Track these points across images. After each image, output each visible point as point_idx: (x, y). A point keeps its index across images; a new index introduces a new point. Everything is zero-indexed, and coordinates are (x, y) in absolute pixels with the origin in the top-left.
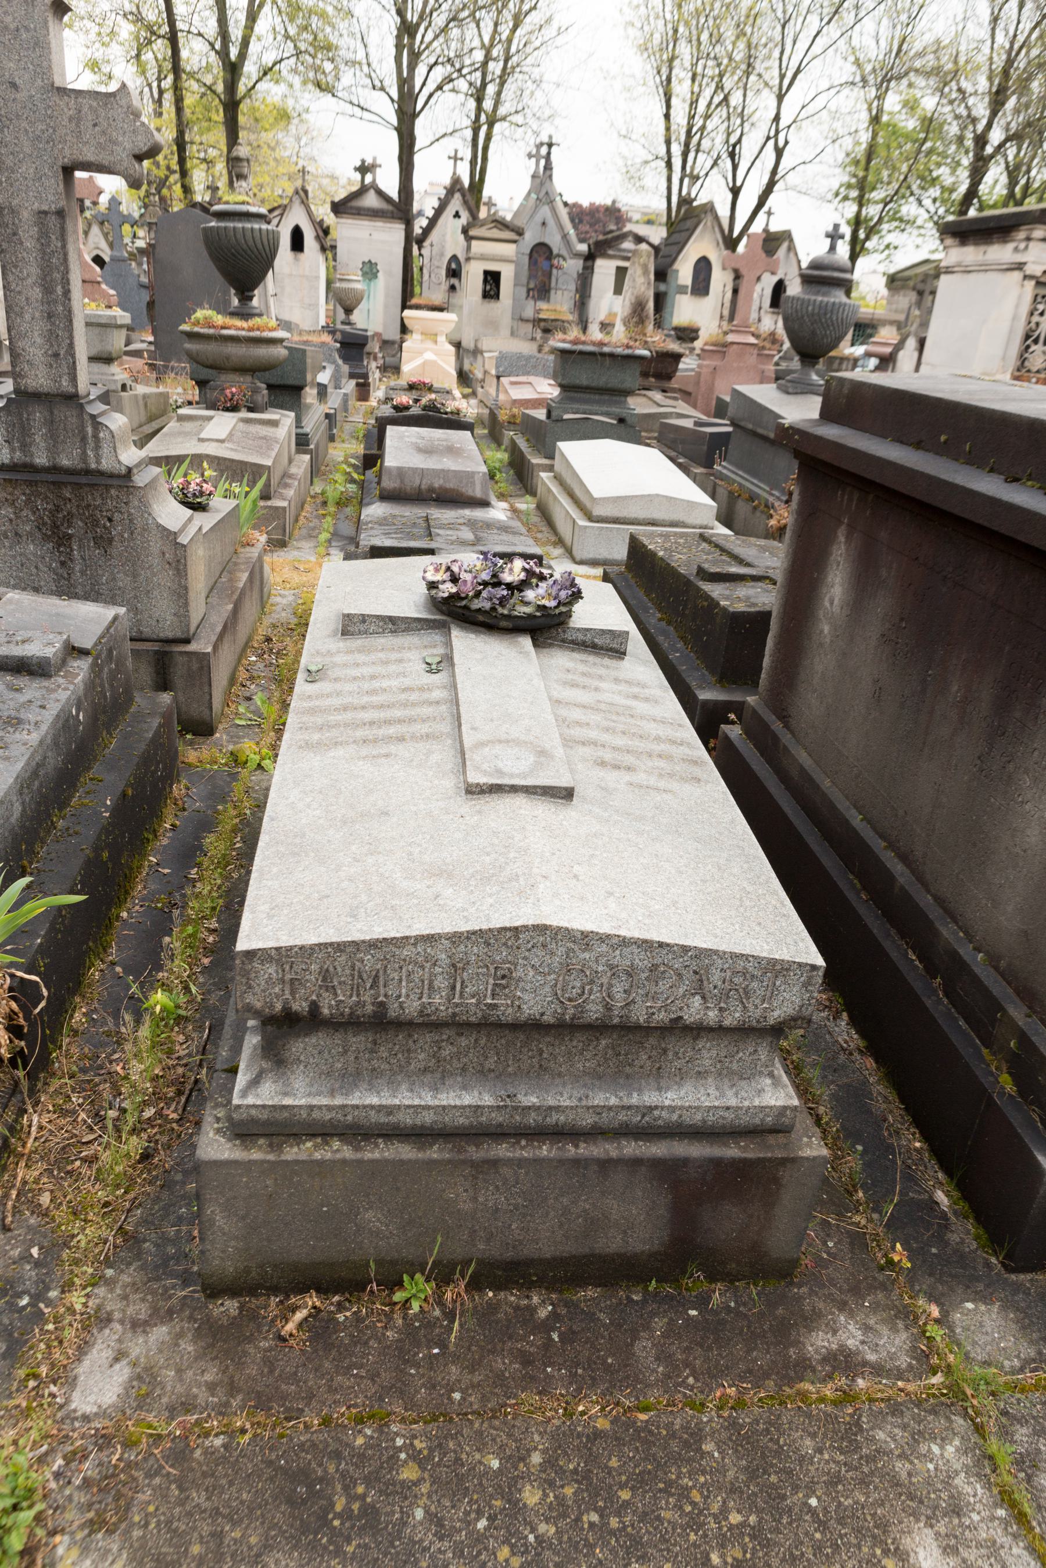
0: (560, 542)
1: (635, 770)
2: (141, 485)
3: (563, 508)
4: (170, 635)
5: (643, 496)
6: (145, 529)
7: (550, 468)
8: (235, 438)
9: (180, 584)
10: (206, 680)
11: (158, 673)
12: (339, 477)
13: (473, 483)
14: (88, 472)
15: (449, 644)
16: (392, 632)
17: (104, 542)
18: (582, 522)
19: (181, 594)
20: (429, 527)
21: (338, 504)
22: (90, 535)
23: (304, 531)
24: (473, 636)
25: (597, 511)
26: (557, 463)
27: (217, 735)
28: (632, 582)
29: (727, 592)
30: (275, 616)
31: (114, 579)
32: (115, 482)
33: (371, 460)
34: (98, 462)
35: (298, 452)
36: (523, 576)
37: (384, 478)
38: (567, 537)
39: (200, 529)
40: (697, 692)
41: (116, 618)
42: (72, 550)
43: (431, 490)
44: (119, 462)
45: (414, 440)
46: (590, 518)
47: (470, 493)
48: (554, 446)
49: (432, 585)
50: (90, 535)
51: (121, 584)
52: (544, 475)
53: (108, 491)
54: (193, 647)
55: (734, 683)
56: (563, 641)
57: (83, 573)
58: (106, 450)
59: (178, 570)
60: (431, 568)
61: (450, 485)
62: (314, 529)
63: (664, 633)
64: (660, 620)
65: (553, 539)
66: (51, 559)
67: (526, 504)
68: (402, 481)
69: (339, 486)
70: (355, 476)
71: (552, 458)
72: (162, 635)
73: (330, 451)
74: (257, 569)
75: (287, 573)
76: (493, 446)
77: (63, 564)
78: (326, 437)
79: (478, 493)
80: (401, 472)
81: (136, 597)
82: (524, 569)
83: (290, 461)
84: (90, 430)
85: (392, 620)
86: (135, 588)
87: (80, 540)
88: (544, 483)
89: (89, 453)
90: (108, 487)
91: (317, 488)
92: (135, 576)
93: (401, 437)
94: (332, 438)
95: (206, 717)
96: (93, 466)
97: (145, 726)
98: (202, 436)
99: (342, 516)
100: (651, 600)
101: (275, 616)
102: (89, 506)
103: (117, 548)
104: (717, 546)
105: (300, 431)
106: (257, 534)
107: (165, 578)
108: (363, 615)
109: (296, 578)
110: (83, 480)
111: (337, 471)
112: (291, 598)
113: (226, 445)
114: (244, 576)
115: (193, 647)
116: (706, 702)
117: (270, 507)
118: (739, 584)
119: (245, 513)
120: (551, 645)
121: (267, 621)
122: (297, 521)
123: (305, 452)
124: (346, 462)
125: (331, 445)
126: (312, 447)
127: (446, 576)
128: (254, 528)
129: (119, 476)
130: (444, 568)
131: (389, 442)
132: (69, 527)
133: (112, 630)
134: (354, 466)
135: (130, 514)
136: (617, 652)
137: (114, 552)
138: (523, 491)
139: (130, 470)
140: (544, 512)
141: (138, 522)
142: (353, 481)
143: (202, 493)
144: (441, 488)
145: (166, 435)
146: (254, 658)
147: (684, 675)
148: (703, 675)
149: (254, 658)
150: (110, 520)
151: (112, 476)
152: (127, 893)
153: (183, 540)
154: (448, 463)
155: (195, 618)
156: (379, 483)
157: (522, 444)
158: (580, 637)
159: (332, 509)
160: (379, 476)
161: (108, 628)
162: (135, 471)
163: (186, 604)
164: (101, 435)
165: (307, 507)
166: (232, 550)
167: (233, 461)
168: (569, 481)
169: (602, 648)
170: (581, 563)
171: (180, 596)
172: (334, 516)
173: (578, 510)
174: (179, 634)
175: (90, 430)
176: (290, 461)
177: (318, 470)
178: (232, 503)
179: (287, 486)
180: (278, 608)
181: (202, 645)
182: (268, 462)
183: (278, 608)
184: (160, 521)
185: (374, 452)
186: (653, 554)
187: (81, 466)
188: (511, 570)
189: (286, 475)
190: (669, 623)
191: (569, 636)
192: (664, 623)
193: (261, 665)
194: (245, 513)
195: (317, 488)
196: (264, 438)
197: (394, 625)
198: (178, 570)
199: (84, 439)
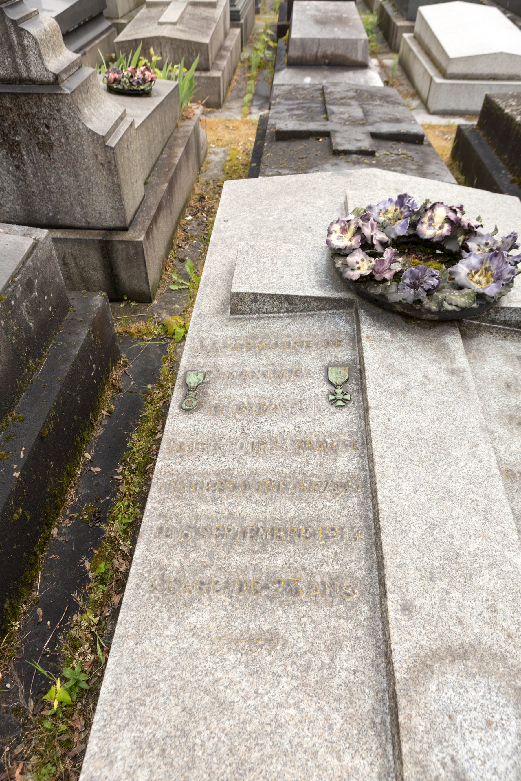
0: (417, 94)
2: (68, 92)
3: (422, 65)
4: (111, 224)
5: (489, 55)
6: (78, 134)
7: (411, 29)
8: (184, 21)
9: (113, 182)
10: (142, 262)
11: (104, 257)
12: (259, 45)
13: (356, 49)
14: (21, 81)
15: (356, 340)
16: (288, 311)
17: (46, 147)
18: (438, 80)
19: (116, 191)
20: (324, 103)
21: (259, 67)
22: (33, 141)
23: (235, 92)
24: (387, 335)
25: (452, 69)
26: (417, 25)
27: (155, 302)
28: (484, 139)
30: (209, 173)
31: (60, 179)
32: (45, 90)
33: (283, 30)
34: (28, 71)
35: (233, 26)
36: (446, 229)
37: (291, 48)
38: (424, 92)
39: (132, 125)
41: (34, 247)
42: (22, 155)
43: (325, 56)
44: (46, 70)
45: (313, 12)
46: (444, 74)
47: (354, 57)
48: (416, 11)
49: (338, 253)
50: (33, 141)
51: (66, 183)
52: (406, 36)
53: (41, 100)
54: (129, 236)
57: (35, 174)
58: (32, 58)
59: (110, 170)
60: (337, 227)
61: (339, 52)
62: (241, 90)
64: (512, 182)
65: (412, 91)
66: (7, 164)
67: (391, 61)
68: (304, 50)
69: (259, 52)
70: (271, 44)
71: (413, 20)
72: (105, 225)
73: (257, 22)
74: (193, 139)
75: (221, 132)
76: (368, 12)
77: (17, 167)
78: (253, 10)
79: (359, 57)
80: (303, 42)
81: (80, 194)
82: (448, 220)
83: (226, 35)
84: (14, 37)
85: (288, 299)
86: (78, 187)
87: (27, 146)
88: (406, 43)
89: (19, 61)
90: (40, 96)
91: (246, 54)
92: (76, 176)
93: (304, 11)
94: (257, 11)
95: (146, 290)
96: (25, 75)
97: (74, 338)
98: (162, 20)
99: (261, 78)
100: (504, 161)
101: (209, 173)
102: (27, 114)
103: (58, 152)
105: (234, 9)
106: (194, 106)
107: (100, 178)
108: (255, 294)
109: (227, 137)
110: (18, 89)
111: (259, 40)
112: (221, 155)
113: (178, 27)
114: (180, 151)
115: (129, 236)
117: (209, 78)
119: (183, 92)
121: (203, 179)
122: (229, 84)
123: (237, 26)
124: (265, 32)
125: (257, 17)
126: (242, 21)
127: (355, 242)
128: (192, 101)
129: (48, 84)
130: (353, 228)
131: (295, 16)
132: (15, 135)
133: (29, 263)
134: (271, 36)
135: (63, 121)
137: (56, 156)
138: (388, 49)
139: (57, 77)
140: (404, 67)
141: (71, 128)
142: (269, 48)
143: (144, 80)
144: (332, 54)
145: (138, 20)
146: (190, 218)
149: (190, 218)
150: (48, 127)
151: (42, 83)
152: (57, 508)
153: (112, 142)
154: (338, 33)
155: (131, 205)
156: (287, 51)
157: (389, 9)
159: (254, 73)
160: (288, 44)
161: (23, 262)
162: (64, 77)
163: (121, 199)
164: (26, 42)
165: (238, 72)
166: (174, 125)
167: (181, 41)
168: (427, 41)
170: (434, 113)
171: (114, 193)
172: (256, 79)
173: (434, 68)
174: (118, 224)
175: (14, 37)
176: (226, 35)
177: (247, 39)
178: (173, 84)
179: (222, 57)
180: (212, 166)
181: (136, 235)
182: (206, 40)
183: (212, 166)
184: (90, 126)
185: (285, 23)
186: (510, 119)
187: (14, 75)
188: (431, 219)
189: (222, 48)
193: (194, 224)
194: (183, 92)
195: (246, 54)
196: (205, 18)
197: (292, 305)
198: (110, 170)
199: (11, 47)
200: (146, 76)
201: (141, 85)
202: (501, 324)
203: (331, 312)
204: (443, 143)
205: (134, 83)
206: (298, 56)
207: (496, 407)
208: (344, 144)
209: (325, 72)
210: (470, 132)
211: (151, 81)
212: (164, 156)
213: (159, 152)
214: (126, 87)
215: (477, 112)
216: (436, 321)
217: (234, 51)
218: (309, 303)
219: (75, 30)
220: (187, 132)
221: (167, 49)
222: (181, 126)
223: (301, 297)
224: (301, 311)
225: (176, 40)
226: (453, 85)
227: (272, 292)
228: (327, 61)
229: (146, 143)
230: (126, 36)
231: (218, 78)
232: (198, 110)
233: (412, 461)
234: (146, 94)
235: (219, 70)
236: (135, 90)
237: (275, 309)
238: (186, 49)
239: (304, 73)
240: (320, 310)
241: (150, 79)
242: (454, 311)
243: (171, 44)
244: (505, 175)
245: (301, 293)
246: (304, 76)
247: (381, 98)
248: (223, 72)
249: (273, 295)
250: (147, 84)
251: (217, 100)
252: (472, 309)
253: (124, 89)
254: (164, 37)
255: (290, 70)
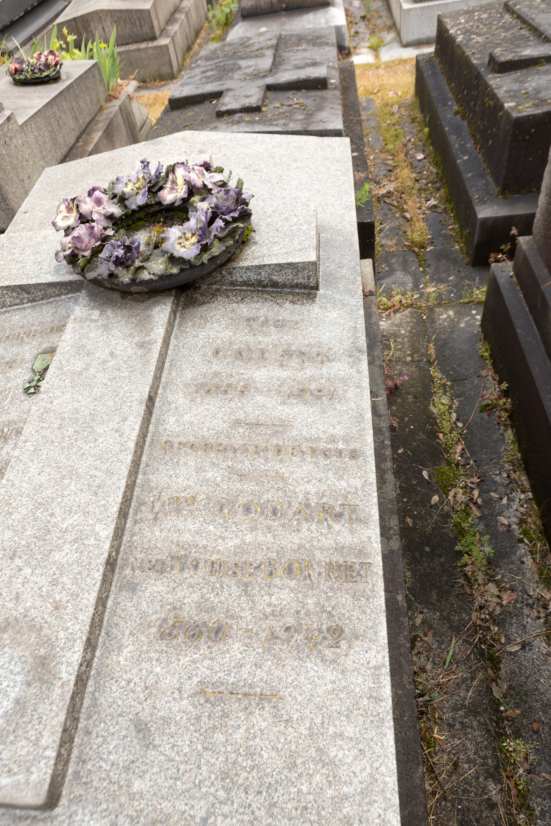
1: (218, 633)
16: (30, 301)
28: (439, 67)
29: (515, 87)
40: (477, 208)
55: (518, 192)
56: (233, 284)
63: (457, 130)
64: (456, 113)
104: (519, 17)
116: (485, 221)
118: (533, 70)
119: (107, 65)
120: (214, 295)
136: (305, 287)
147: (468, 185)
148: (487, 184)
158: (253, 277)
167: (121, 11)
169: (284, 286)
182: (147, 6)
188: (174, 182)
190: (463, 117)
191: (238, 277)
192: (459, 117)
200: (49, 60)
201: (43, 71)
202: (242, 286)
203: (69, 296)
204: (362, 83)
205: (36, 71)
206: (252, 6)
207: (190, 376)
208: (230, 103)
209: (283, 19)
210: (427, 62)
211: (56, 65)
212: (80, 144)
213: (72, 141)
214: (29, 76)
215: (432, 38)
216: (146, 293)
217: (193, 11)
218: (45, 290)
219: (21, 18)
220: (111, 113)
221: (108, 23)
222: (106, 108)
223: (33, 285)
224: (42, 299)
225: (115, 11)
226: (424, 8)
227: (7, 284)
228: (284, 6)
229: (47, 134)
230: (66, 16)
231: (166, 46)
232: (130, 86)
233: (53, 442)
234: (56, 79)
235: (168, 37)
236: (38, 78)
237: (18, 301)
238: (128, 20)
239: (260, 24)
240: (59, 295)
241: (53, 63)
242: (151, 280)
243: (112, 17)
244: (452, 105)
245: (34, 282)
246: (260, 27)
247: (308, 42)
248: (173, 38)
249: (7, 287)
250: (52, 70)
251: (169, 71)
252: (171, 275)
253: (26, 79)
254: (102, 11)
255: (245, 23)
